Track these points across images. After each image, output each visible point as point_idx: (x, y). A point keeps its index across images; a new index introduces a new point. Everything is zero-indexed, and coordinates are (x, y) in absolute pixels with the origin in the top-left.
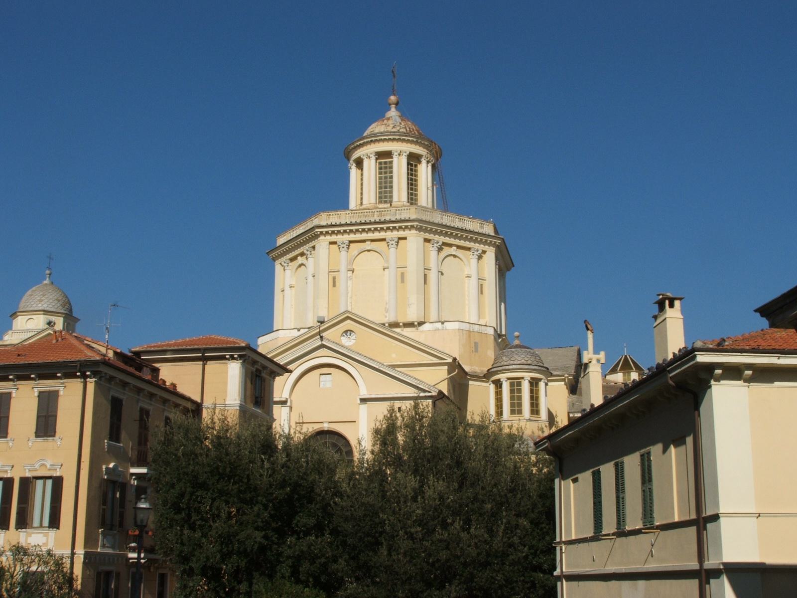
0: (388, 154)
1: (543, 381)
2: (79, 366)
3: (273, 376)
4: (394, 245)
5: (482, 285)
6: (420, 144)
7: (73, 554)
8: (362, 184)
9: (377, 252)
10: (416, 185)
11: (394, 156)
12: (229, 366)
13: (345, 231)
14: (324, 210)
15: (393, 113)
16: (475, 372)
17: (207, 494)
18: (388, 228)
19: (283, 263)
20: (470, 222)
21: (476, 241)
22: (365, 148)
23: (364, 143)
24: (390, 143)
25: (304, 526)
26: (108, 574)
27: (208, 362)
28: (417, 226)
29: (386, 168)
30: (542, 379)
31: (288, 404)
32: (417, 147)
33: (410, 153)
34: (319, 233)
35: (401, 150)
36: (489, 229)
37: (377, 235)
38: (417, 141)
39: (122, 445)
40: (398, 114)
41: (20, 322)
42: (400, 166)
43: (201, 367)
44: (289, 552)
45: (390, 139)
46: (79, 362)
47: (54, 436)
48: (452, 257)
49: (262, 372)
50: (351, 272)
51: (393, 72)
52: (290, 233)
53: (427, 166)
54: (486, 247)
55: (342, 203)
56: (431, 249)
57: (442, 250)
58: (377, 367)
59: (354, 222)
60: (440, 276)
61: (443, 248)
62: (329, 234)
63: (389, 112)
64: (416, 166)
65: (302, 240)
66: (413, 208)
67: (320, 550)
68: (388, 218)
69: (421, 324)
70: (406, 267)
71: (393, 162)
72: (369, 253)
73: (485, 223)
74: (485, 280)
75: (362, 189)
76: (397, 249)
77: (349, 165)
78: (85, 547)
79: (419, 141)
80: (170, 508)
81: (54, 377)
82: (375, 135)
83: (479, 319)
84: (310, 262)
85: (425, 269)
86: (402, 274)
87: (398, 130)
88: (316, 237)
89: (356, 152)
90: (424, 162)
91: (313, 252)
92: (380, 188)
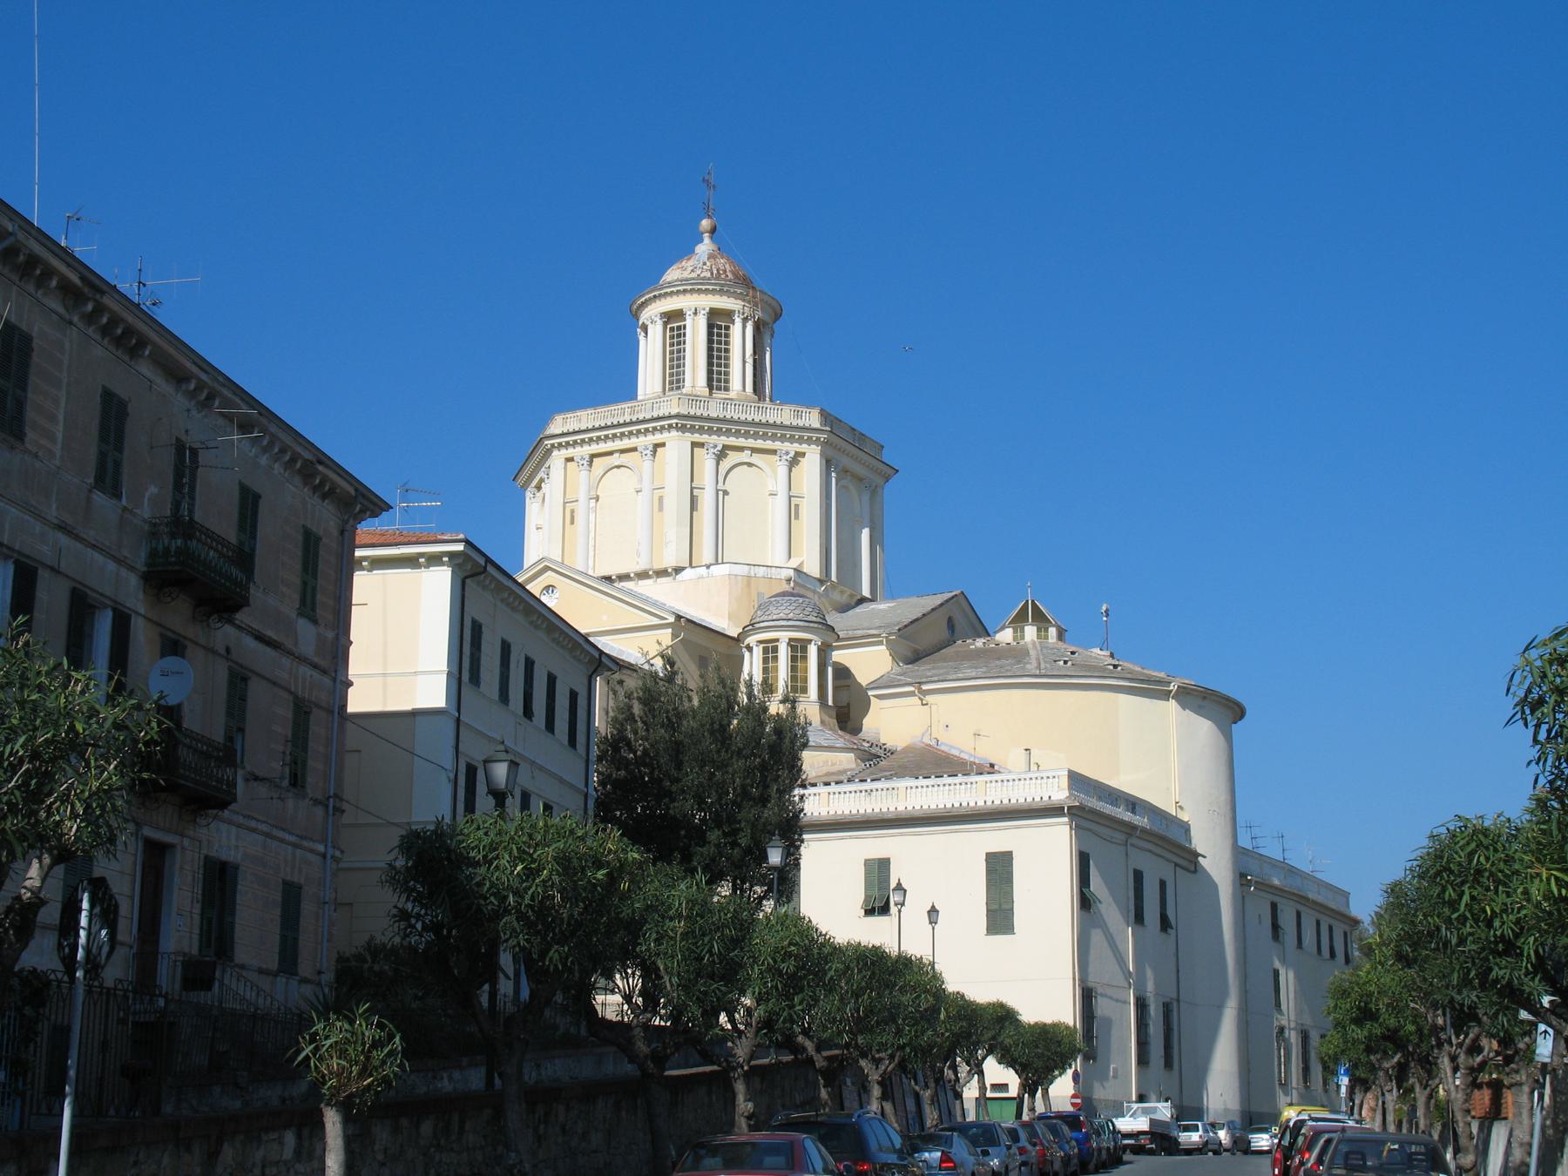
0: (678, 315)
1: (813, 643)
4: (649, 455)
6: (729, 294)
11: (687, 317)
15: (705, 247)
18: (639, 432)
21: (783, 439)
30: (811, 640)
36: (812, 419)
37: (626, 443)
48: (746, 466)
50: (594, 501)
54: (804, 446)
62: (571, 445)
63: (700, 245)
64: (727, 328)
66: (673, 397)
69: (678, 570)
70: (663, 488)
74: (803, 497)
76: (654, 461)
79: (725, 289)
83: (790, 557)
86: (661, 499)
87: (699, 275)
90: (738, 321)
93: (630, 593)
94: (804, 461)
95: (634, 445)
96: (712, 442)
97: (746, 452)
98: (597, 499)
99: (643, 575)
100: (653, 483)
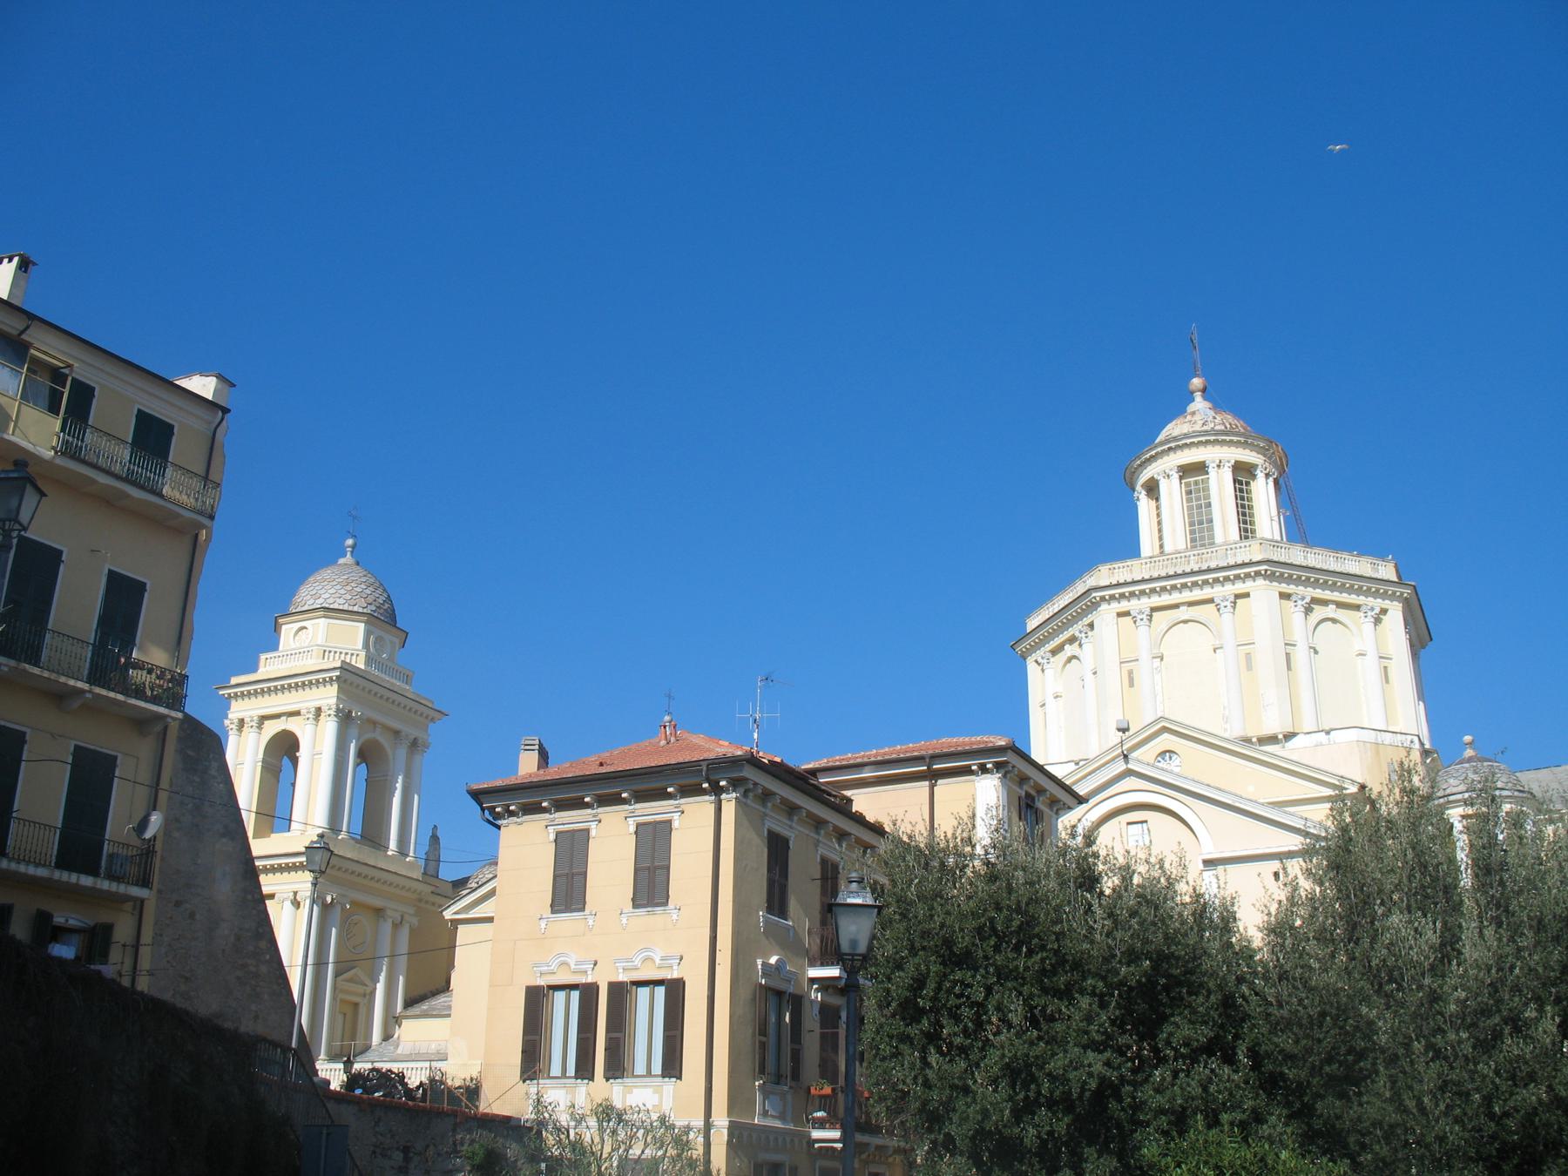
0: (1200, 468)
2: (705, 768)
3: (1055, 809)
4: (1229, 607)
5: (1385, 668)
7: (708, 1126)
8: (1159, 523)
9: (1201, 623)
10: (1252, 515)
12: (977, 784)
13: (1143, 593)
14: (1105, 561)
15: (1199, 404)
17: (973, 977)
18: (1216, 580)
19: (1040, 660)
20: (1353, 562)
21: (1368, 593)
22: (1160, 461)
24: (1202, 449)
25: (1186, 1045)
27: (940, 782)
28: (1266, 572)
32: (1247, 452)
34: (1098, 599)
36: (1387, 571)
37: (1197, 594)
38: (1246, 442)
39: (791, 923)
40: (1208, 405)
42: (1221, 485)
43: (926, 790)
44: (1161, 1100)
45: (1202, 441)
46: (706, 763)
47: (666, 903)
48: (1330, 623)
49: (1036, 799)
50: (1159, 660)
52: (1048, 608)
53: (1267, 483)
54: (1387, 602)
55: (1129, 548)
56: (1292, 610)
57: (1311, 612)
58: (1230, 802)
59: (1155, 575)
60: (1312, 654)
61: (1313, 608)
63: (1192, 405)
64: (1248, 484)
65: (1071, 615)
67: (1231, 1094)
68: (1213, 565)
69: (1289, 736)
70: (1254, 643)
71: (1210, 480)
72: (1186, 625)
73: (1381, 563)
74: (1391, 659)
75: (1160, 531)
77: (1136, 494)
78: (730, 1114)
79: (1250, 441)
80: (893, 1016)
81: (662, 795)
82: (1175, 439)
84: (1087, 652)
85: (1286, 644)
86: (1248, 656)
88: (1095, 605)
89: (1145, 471)
90: (1260, 475)
91: (1090, 633)
92: (1192, 524)
95: (1210, 596)
96: (1301, 593)
97: (1330, 606)
100: (314, 747)
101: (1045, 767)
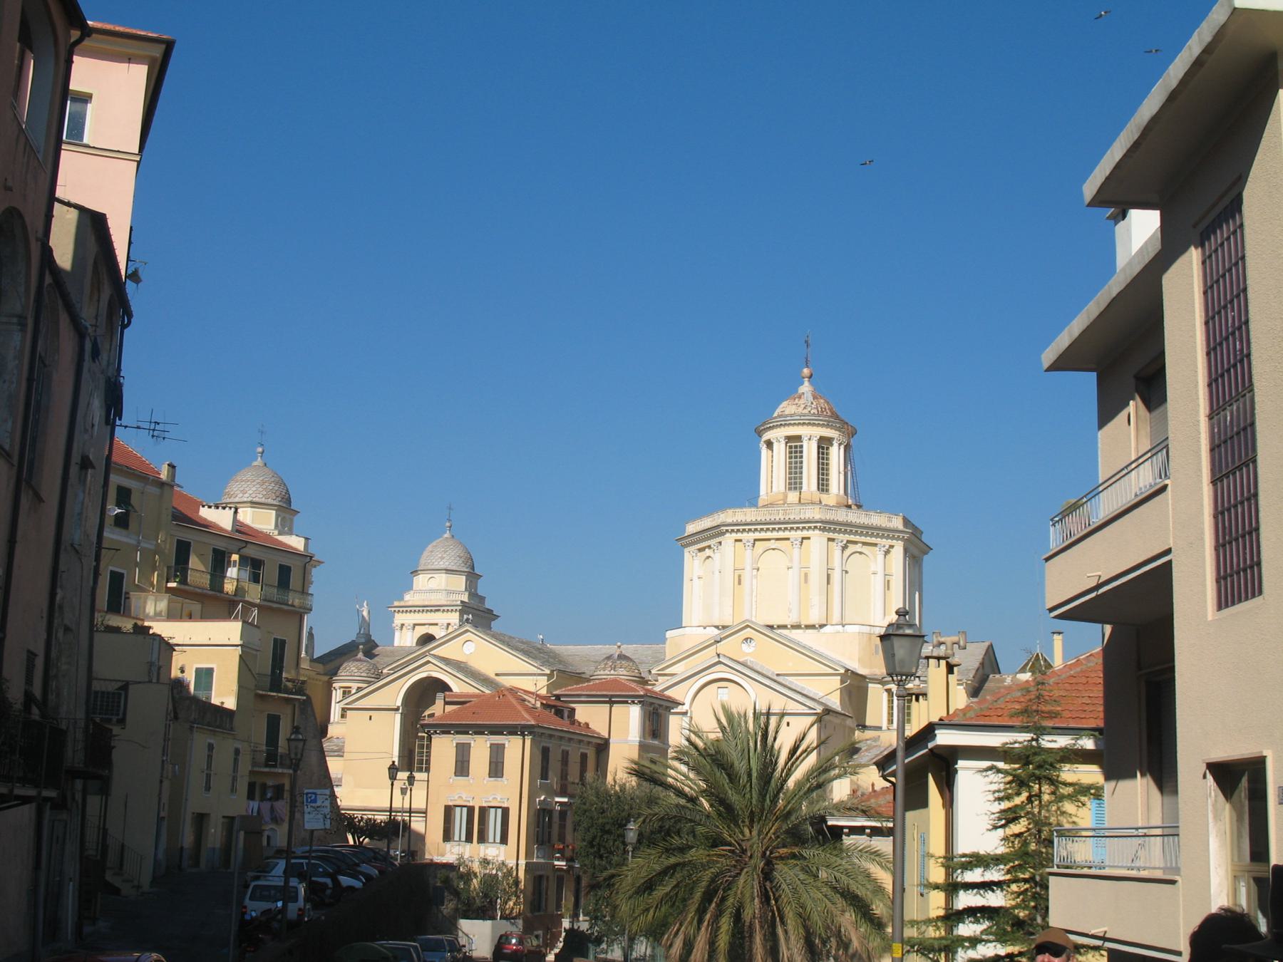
0: (799, 438)
5: (888, 581)
6: (832, 427)
12: (631, 708)
13: (750, 530)
15: (806, 388)
16: (876, 675)
21: (882, 537)
23: (774, 426)
26: (541, 877)
29: (796, 452)
31: (689, 715)
33: (821, 437)
35: (810, 435)
36: (897, 523)
37: (781, 534)
41: (421, 581)
42: (810, 451)
43: (608, 708)
47: (502, 777)
48: (858, 554)
51: (806, 342)
53: (839, 449)
54: (895, 541)
55: (750, 497)
63: (801, 387)
64: (828, 448)
69: (822, 626)
71: (804, 447)
78: (526, 859)
81: (501, 734)
84: (717, 556)
86: (806, 575)
88: (723, 534)
90: (836, 444)
91: (719, 547)
93: (785, 637)
94: (893, 551)
98: (758, 570)
99: (797, 627)
101: (668, 693)
